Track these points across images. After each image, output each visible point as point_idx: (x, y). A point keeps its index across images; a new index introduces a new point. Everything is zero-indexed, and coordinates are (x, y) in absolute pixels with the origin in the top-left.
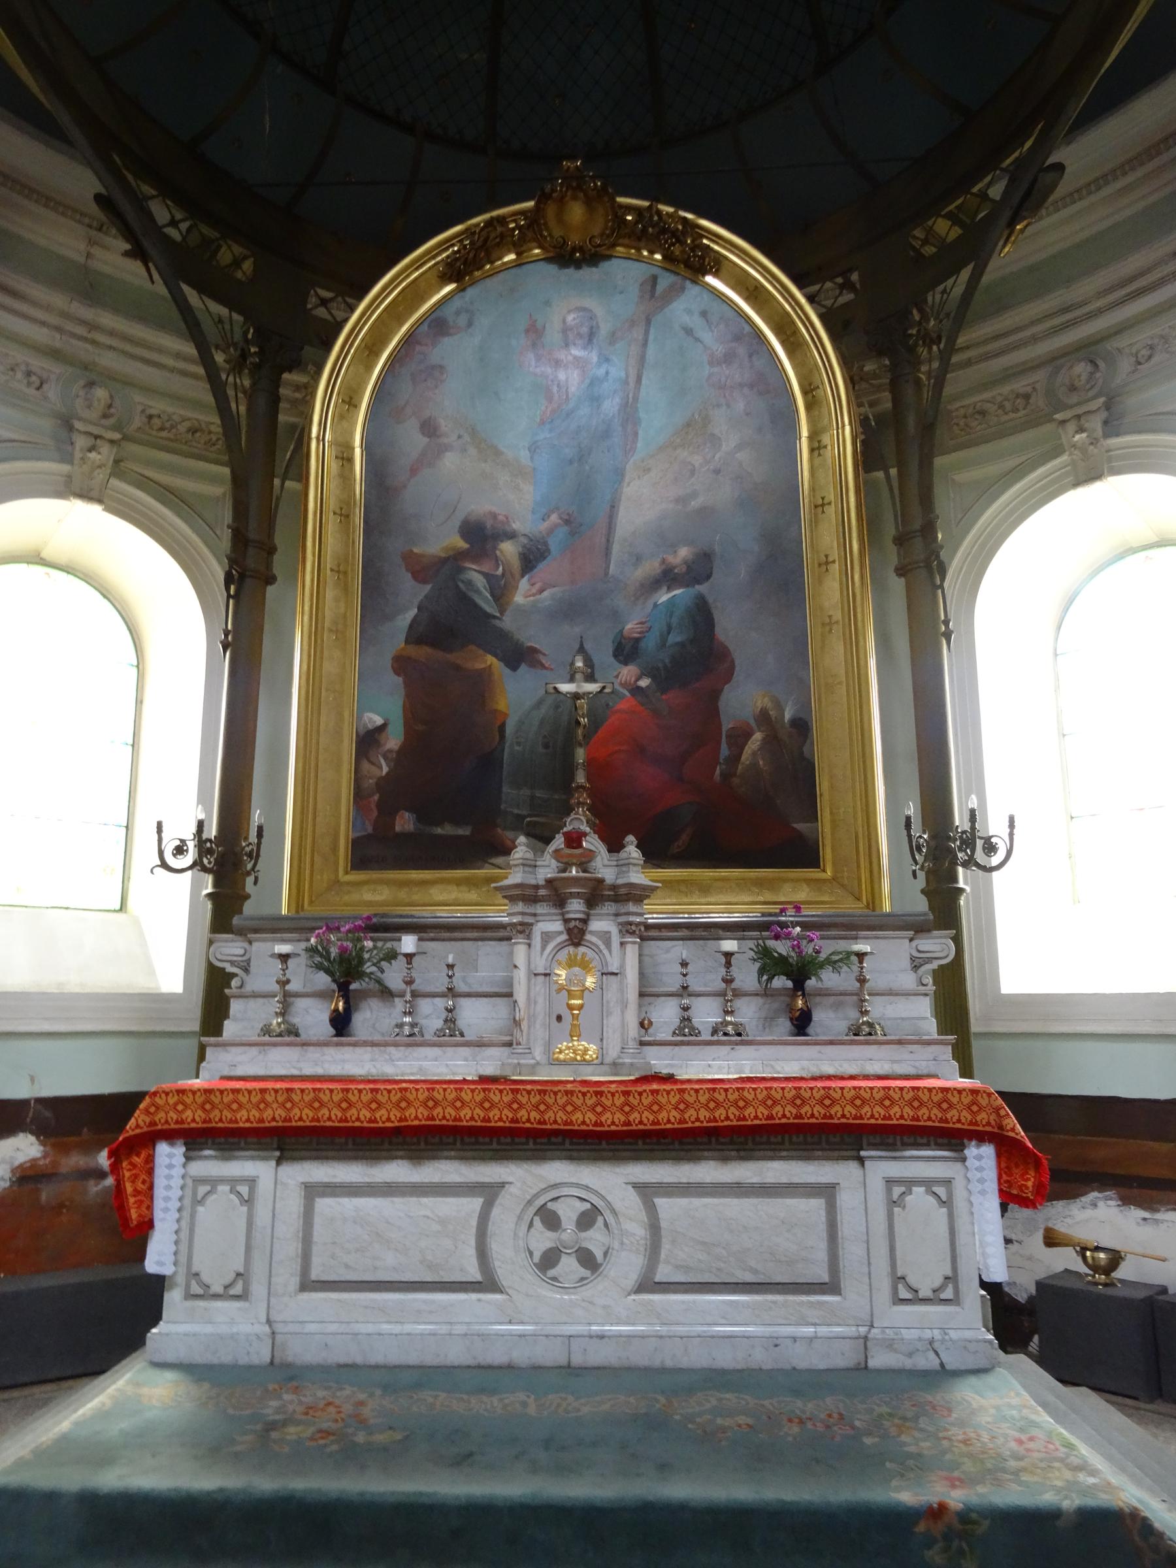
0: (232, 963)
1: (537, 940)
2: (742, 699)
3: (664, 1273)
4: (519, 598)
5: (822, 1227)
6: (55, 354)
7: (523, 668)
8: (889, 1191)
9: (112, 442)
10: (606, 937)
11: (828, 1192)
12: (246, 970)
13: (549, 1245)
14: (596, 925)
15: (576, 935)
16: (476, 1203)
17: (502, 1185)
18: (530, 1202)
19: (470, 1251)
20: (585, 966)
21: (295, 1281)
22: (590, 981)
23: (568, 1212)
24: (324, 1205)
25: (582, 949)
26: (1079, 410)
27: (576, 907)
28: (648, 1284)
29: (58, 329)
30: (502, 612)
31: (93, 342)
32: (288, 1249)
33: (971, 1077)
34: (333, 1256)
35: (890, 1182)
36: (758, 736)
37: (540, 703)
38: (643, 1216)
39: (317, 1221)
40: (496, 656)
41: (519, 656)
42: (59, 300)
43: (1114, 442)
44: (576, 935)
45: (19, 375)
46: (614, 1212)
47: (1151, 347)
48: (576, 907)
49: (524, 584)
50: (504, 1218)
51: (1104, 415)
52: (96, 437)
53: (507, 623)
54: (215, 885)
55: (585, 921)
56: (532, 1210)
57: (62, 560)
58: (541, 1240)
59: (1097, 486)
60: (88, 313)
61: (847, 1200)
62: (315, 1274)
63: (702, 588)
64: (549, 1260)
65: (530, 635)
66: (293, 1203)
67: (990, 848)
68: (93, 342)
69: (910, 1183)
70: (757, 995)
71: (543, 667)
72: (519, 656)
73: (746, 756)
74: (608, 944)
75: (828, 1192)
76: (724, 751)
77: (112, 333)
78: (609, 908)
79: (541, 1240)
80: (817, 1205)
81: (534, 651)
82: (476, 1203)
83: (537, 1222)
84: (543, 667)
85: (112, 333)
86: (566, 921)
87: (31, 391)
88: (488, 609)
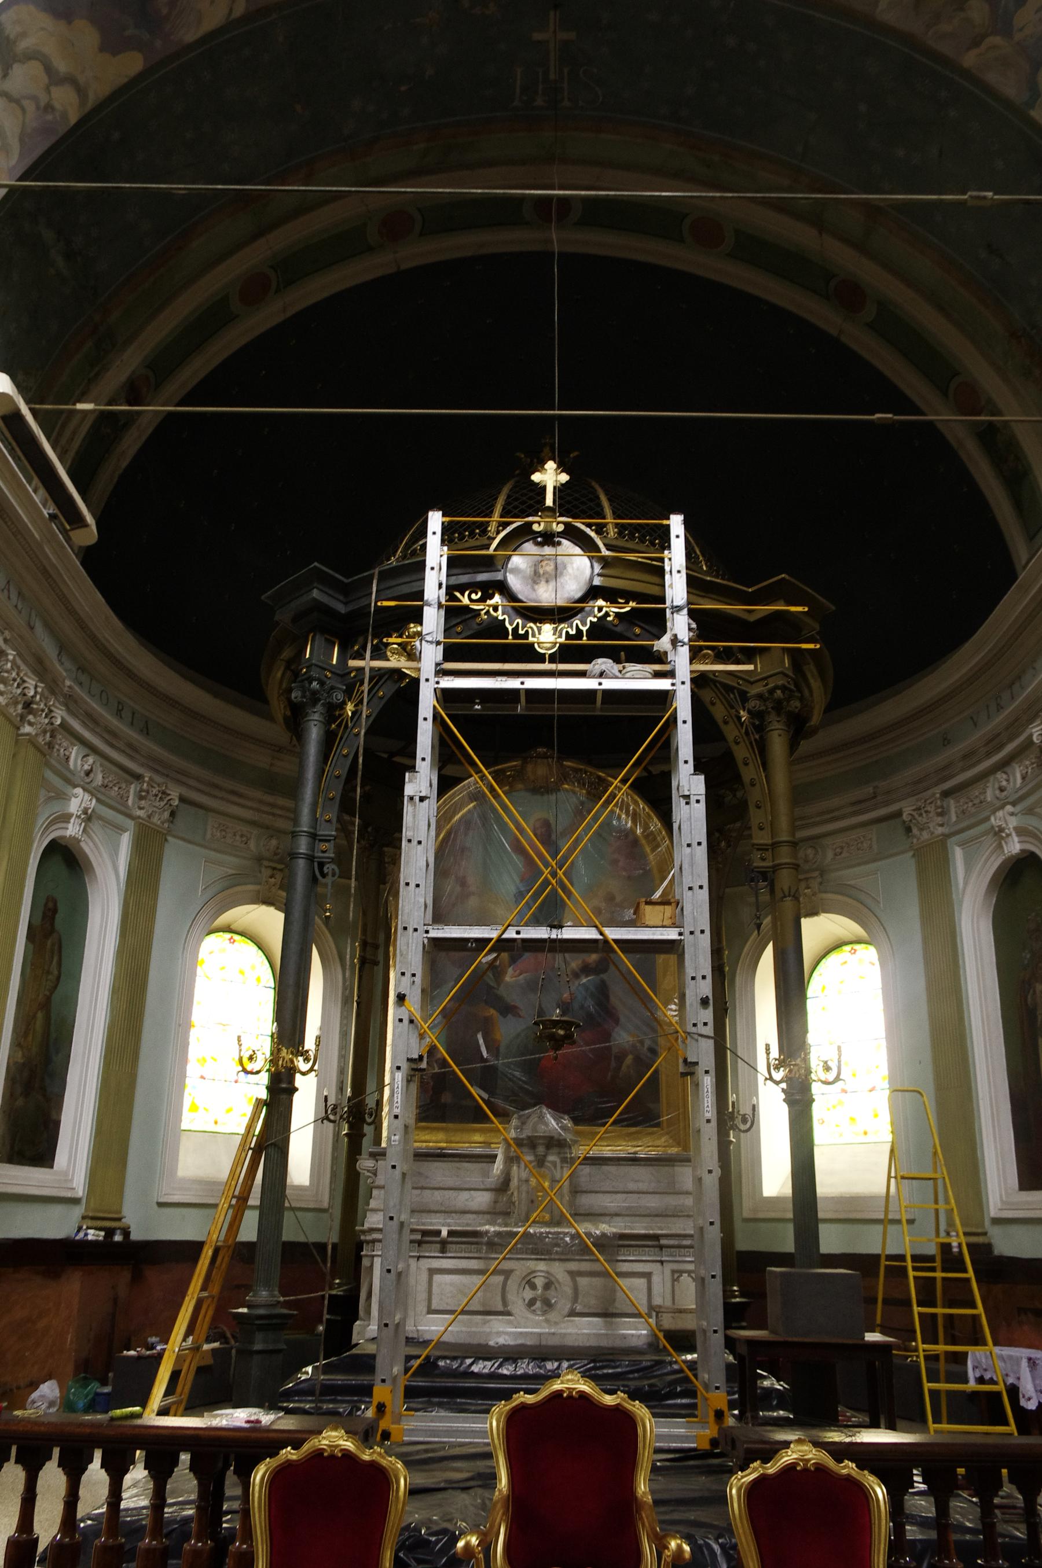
0: (368, 1171)
1: (522, 1165)
2: (623, 1037)
3: (579, 1308)
4: (508, 979)
5: (645, 1290)
6: (253, 823)
7: (510, 1016)
8: (673, 1276)
9: (281, 870)
10: (554, 1164)
11: (648, 1276)
12: (375, 1175)
13: (531, 1296)
14: (551, 1158)
15: (541, 1162)
16: (501, 1278)
17: (512, 1271)
18: (524, 1278)
19: (499, 1298)
20: (543, 1177)
21: (425, 1310)
22: (546, 1184)
23: (539, 1282)
24: (437, 1278)
25: (543, 1169)
26: (808, 875)
27: (541, 1150)
28: (573, 1313)
29: (258, 810)
30: (499, 985)
31: (273, 815)
32: (422, 1296)
33: (496, 1156)
34: (441, 1299)
35: (673, 1272)
36: (630, 1057)
37: (519, 1035)
38: (571, 1284)
39: (434, 1285)
40: (494, 1008)
41: (507, 1010)
42: (258, 794)
43: (824, 896)
44: (541, 1162)
45: (238, 838)
46: (559, 1283)
47: (842, 848)
48: (541, 1150)
49: (510, 970)
50: (512, 1284)
51: (819, 880)
52: (274, 869)
53: (502, 991)
54: (350, 1128)
55: (545, 1156)
56: (524, 1282)
57: (240, 929)
58: (528, 1294)
59: (815, 918)
60: (270, 799)
61: (656, 1279)
62: (435, 1306)
63: (604, 976)
64: (531, 1303)
65: (513, 998)
66: (424, 1277)
67: (744, 1120)
68: (273, 815)
69: (681, 1272)
70: (484, 1213)
71: (520, 1016)
72: (507, 1010)
73: (624, 1068)
74: (555, 1167)
75: (648, 1276)
76: (613, 1064)
77: (282, 808)
78: (555, 1150)
79: (528, 1294)
80: (642, 1282)
81: (515, 1007)
82: (501, 1278)
83: (527, 1287)
84: (520, 1016)
85: (282, 808)
86: (536, 1156)
87: (243, 845)
88: (492, 984)
